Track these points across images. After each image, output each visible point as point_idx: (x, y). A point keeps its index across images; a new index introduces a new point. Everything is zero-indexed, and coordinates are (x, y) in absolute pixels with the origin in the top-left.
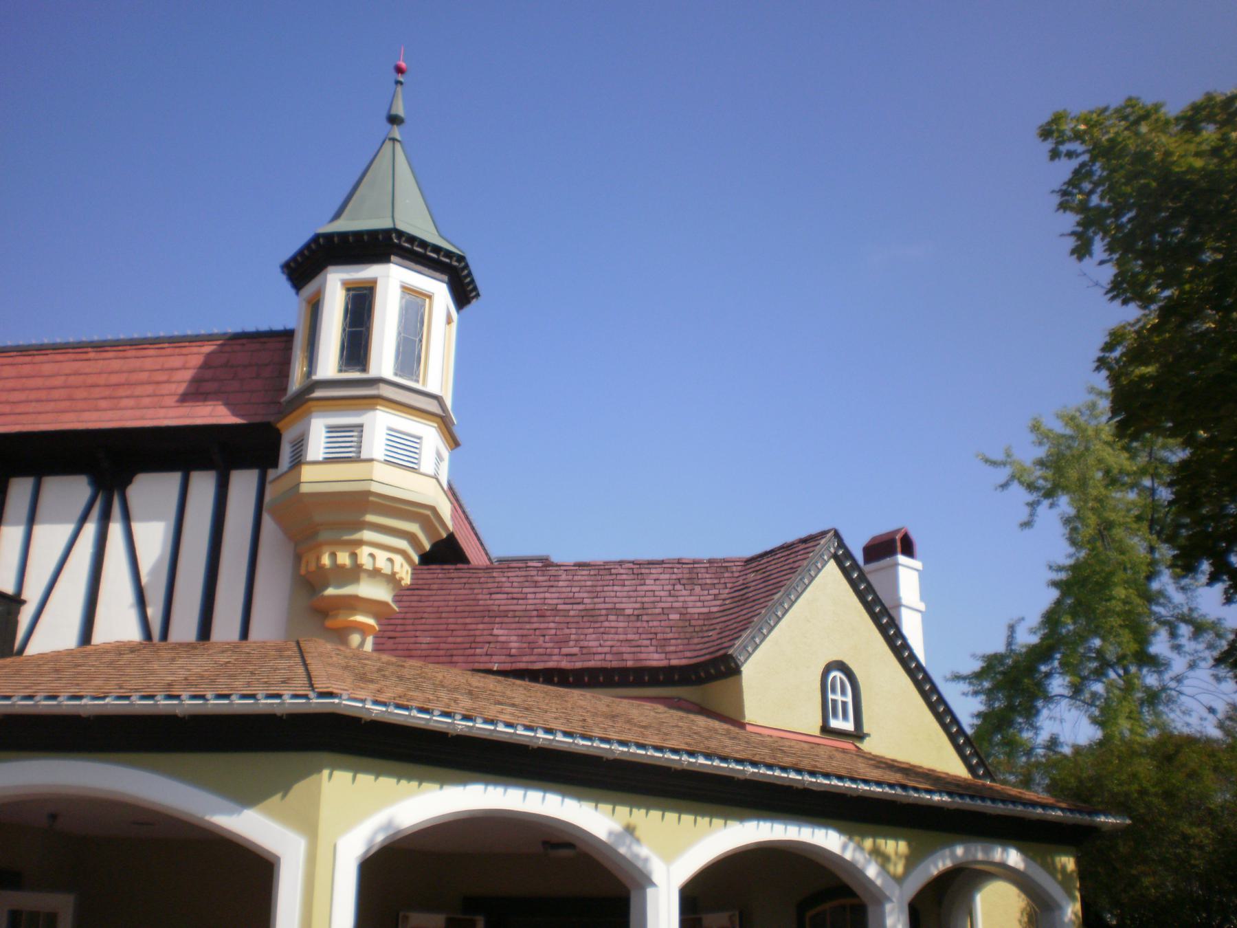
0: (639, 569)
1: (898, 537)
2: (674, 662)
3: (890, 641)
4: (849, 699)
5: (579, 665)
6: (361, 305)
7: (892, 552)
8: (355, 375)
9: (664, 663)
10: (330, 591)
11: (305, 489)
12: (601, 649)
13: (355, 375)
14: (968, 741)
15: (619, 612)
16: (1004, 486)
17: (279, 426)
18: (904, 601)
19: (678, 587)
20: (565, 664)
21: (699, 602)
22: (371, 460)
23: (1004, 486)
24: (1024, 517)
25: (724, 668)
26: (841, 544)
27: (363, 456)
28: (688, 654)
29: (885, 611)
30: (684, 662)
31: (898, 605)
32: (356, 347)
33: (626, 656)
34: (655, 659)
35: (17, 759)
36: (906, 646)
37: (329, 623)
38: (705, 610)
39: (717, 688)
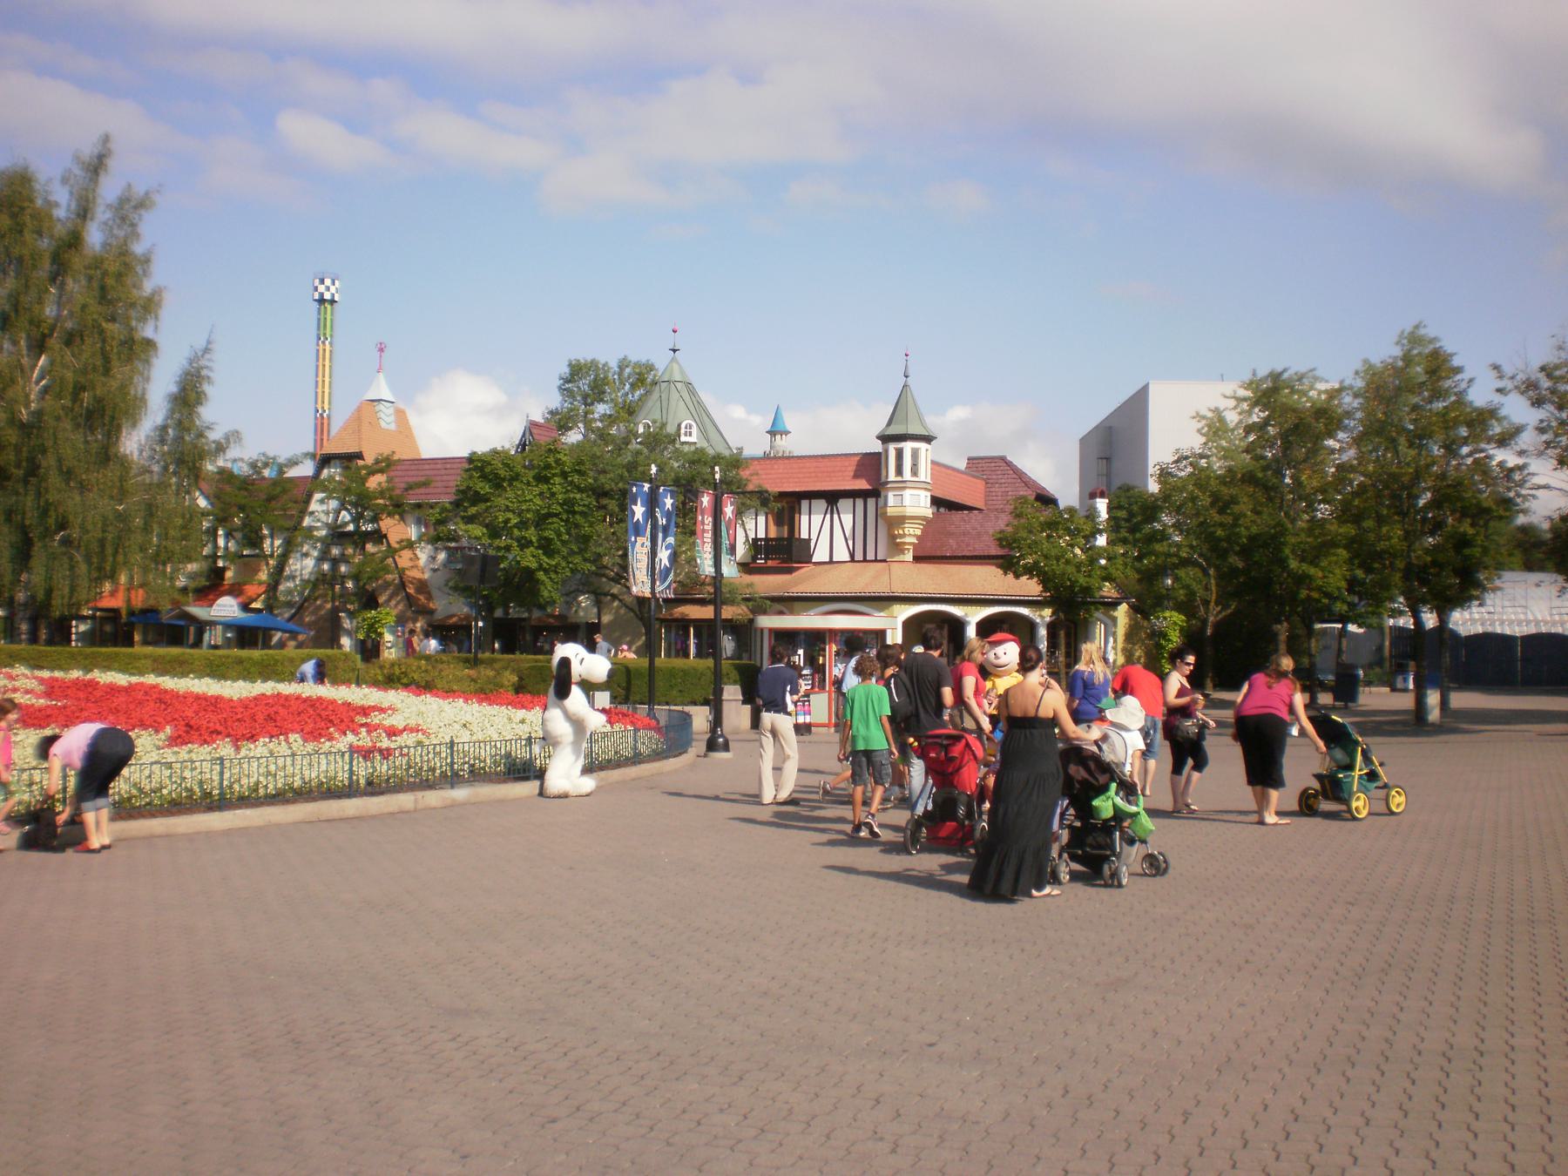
6: (900, 453)
16: (96, 167)
32: (899, 471)
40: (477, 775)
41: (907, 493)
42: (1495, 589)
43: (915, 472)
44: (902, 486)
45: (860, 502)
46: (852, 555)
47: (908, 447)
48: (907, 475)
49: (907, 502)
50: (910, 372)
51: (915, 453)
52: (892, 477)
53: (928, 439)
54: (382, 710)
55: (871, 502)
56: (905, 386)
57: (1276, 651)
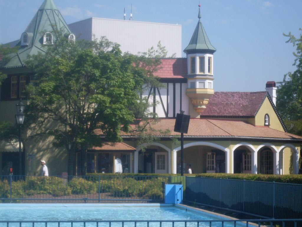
0: (233, 94)
1: (273, 84)
2: (244, 115)
3: (270, 102)
4: (268, 119)
5: (229, 115)
6: (202, 60)
7: (272, 86)
8: (202, 73)
9: (242, 115)
10: (199, 107)
11: (197, 93)
12: (232, 111)
13: (202, 73)
14: (275, 107)
15: (232, 104)
16: (287, 42)
17: (188, 79)
18: (273, 96)
19: (240, 99)
20: (227, 115)
21: (245, 102)
22: (207, 89)
23: (287, 42)
24: (294, 63)
25: (253, 117)
26: (268, 94)
27: (205, 88)
28: (246, 114)
29: (270, 97)
30: (245, 115)
31: (272, 97)
32: (202, 69)
33: (236, 114)
34: (241, 114)
35: (193, 142)
36: (273, 102)
37: (197, 111)
38: (246, 104)
39: (250, 119)
40: (231, 179)
41: (207, 82)
42: (20, 181)
43: (209, 71)
44: (204, 78)
45: (171, 86)
46: (167, 114)
47: (207, 56)
48: (206, 72)
49: (207, 86)
50: (201, 15)
51: (209, 59)
52: (198, 72)
53: (212, 52)
54: (110, 196)
55: (183, 84)
56: (199, 23)
57: (225, 177)
